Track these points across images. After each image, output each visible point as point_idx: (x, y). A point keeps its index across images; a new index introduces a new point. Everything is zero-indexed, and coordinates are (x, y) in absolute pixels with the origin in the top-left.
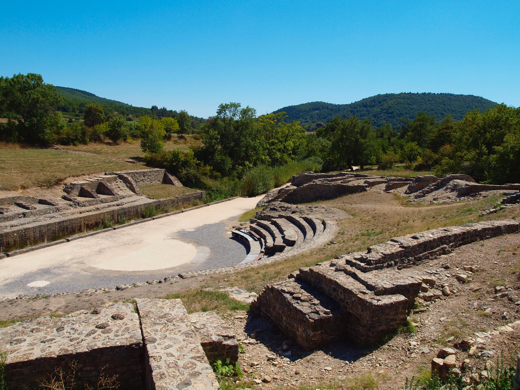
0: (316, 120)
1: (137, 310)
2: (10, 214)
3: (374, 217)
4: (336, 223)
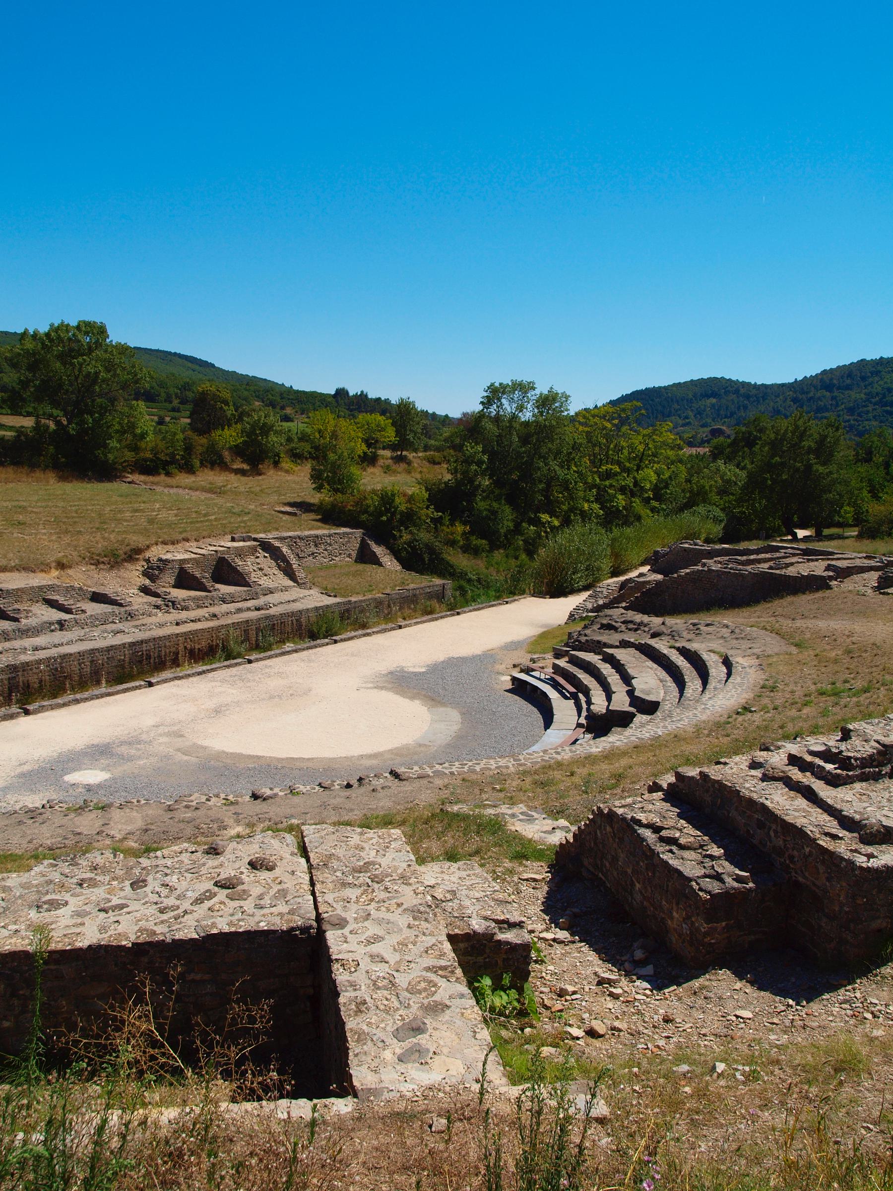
0: (709, 420)
1: (304, 851)
2: (32, 622)
3: (848, 652)
4: (757, 662)
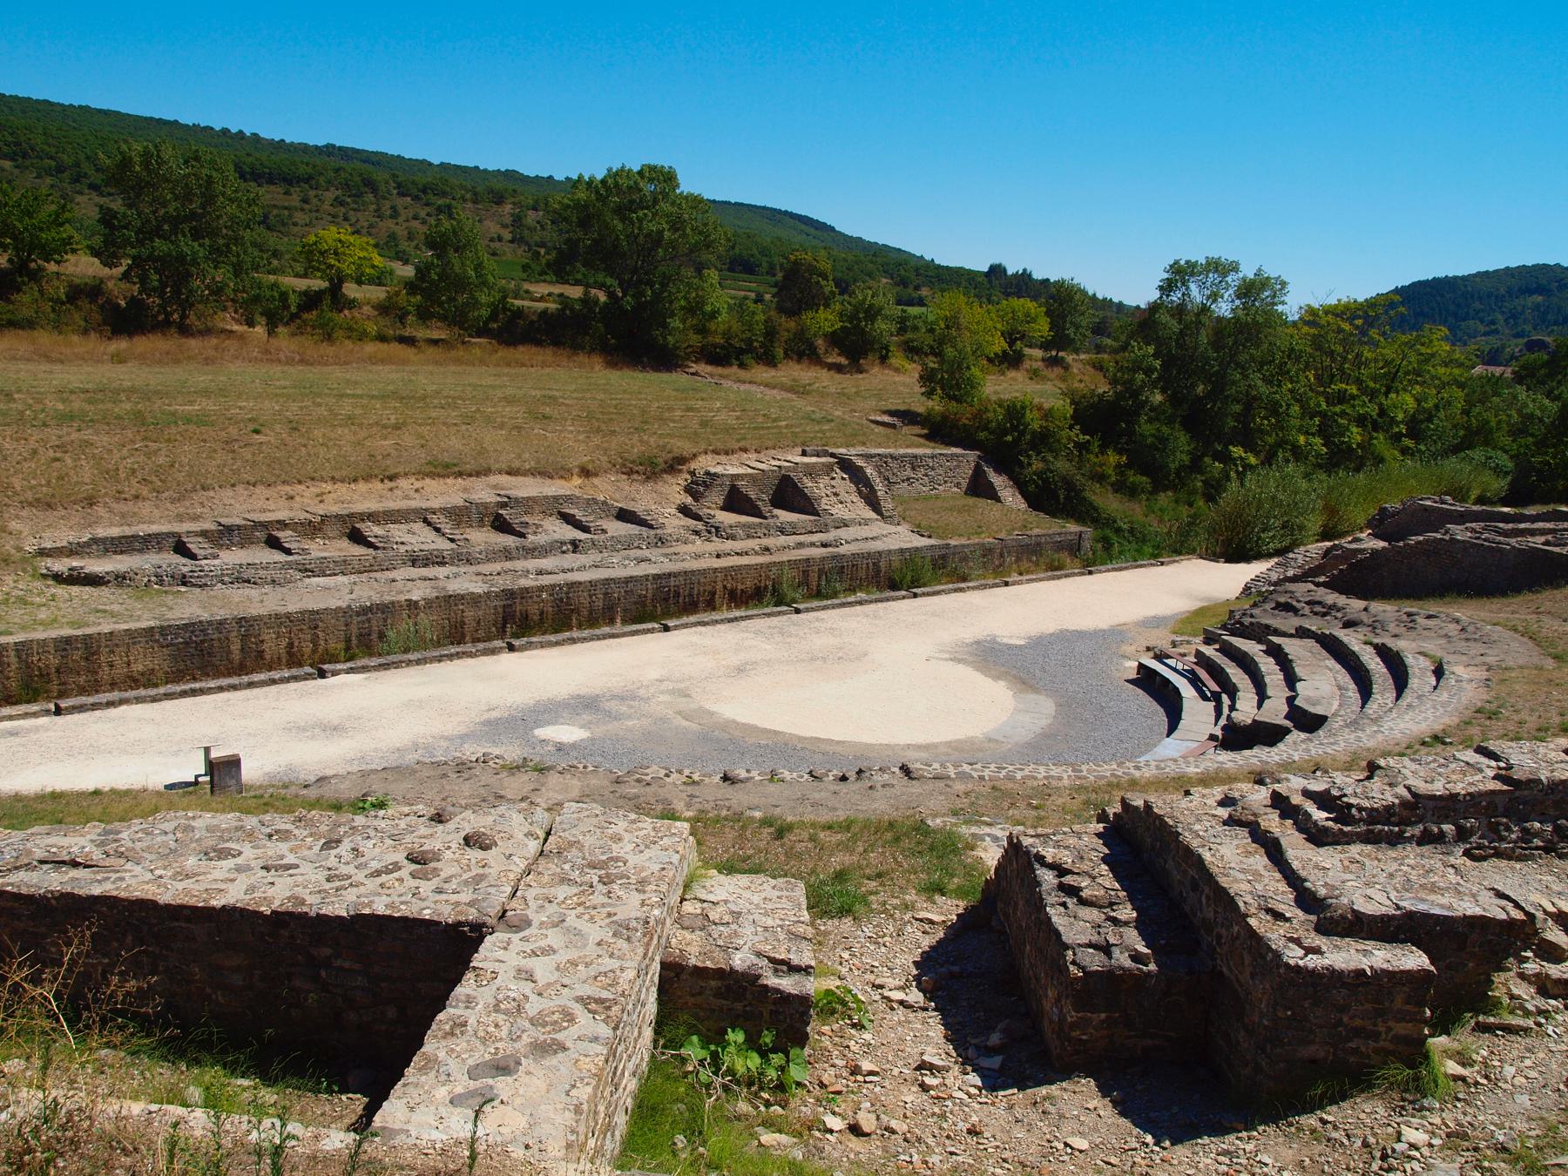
4: (1485, 675)
